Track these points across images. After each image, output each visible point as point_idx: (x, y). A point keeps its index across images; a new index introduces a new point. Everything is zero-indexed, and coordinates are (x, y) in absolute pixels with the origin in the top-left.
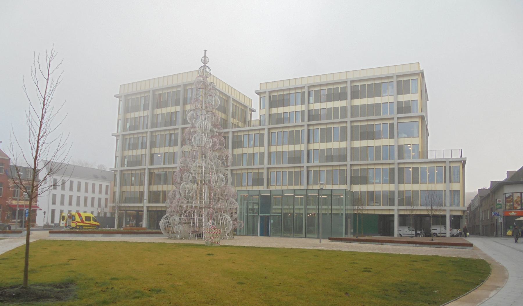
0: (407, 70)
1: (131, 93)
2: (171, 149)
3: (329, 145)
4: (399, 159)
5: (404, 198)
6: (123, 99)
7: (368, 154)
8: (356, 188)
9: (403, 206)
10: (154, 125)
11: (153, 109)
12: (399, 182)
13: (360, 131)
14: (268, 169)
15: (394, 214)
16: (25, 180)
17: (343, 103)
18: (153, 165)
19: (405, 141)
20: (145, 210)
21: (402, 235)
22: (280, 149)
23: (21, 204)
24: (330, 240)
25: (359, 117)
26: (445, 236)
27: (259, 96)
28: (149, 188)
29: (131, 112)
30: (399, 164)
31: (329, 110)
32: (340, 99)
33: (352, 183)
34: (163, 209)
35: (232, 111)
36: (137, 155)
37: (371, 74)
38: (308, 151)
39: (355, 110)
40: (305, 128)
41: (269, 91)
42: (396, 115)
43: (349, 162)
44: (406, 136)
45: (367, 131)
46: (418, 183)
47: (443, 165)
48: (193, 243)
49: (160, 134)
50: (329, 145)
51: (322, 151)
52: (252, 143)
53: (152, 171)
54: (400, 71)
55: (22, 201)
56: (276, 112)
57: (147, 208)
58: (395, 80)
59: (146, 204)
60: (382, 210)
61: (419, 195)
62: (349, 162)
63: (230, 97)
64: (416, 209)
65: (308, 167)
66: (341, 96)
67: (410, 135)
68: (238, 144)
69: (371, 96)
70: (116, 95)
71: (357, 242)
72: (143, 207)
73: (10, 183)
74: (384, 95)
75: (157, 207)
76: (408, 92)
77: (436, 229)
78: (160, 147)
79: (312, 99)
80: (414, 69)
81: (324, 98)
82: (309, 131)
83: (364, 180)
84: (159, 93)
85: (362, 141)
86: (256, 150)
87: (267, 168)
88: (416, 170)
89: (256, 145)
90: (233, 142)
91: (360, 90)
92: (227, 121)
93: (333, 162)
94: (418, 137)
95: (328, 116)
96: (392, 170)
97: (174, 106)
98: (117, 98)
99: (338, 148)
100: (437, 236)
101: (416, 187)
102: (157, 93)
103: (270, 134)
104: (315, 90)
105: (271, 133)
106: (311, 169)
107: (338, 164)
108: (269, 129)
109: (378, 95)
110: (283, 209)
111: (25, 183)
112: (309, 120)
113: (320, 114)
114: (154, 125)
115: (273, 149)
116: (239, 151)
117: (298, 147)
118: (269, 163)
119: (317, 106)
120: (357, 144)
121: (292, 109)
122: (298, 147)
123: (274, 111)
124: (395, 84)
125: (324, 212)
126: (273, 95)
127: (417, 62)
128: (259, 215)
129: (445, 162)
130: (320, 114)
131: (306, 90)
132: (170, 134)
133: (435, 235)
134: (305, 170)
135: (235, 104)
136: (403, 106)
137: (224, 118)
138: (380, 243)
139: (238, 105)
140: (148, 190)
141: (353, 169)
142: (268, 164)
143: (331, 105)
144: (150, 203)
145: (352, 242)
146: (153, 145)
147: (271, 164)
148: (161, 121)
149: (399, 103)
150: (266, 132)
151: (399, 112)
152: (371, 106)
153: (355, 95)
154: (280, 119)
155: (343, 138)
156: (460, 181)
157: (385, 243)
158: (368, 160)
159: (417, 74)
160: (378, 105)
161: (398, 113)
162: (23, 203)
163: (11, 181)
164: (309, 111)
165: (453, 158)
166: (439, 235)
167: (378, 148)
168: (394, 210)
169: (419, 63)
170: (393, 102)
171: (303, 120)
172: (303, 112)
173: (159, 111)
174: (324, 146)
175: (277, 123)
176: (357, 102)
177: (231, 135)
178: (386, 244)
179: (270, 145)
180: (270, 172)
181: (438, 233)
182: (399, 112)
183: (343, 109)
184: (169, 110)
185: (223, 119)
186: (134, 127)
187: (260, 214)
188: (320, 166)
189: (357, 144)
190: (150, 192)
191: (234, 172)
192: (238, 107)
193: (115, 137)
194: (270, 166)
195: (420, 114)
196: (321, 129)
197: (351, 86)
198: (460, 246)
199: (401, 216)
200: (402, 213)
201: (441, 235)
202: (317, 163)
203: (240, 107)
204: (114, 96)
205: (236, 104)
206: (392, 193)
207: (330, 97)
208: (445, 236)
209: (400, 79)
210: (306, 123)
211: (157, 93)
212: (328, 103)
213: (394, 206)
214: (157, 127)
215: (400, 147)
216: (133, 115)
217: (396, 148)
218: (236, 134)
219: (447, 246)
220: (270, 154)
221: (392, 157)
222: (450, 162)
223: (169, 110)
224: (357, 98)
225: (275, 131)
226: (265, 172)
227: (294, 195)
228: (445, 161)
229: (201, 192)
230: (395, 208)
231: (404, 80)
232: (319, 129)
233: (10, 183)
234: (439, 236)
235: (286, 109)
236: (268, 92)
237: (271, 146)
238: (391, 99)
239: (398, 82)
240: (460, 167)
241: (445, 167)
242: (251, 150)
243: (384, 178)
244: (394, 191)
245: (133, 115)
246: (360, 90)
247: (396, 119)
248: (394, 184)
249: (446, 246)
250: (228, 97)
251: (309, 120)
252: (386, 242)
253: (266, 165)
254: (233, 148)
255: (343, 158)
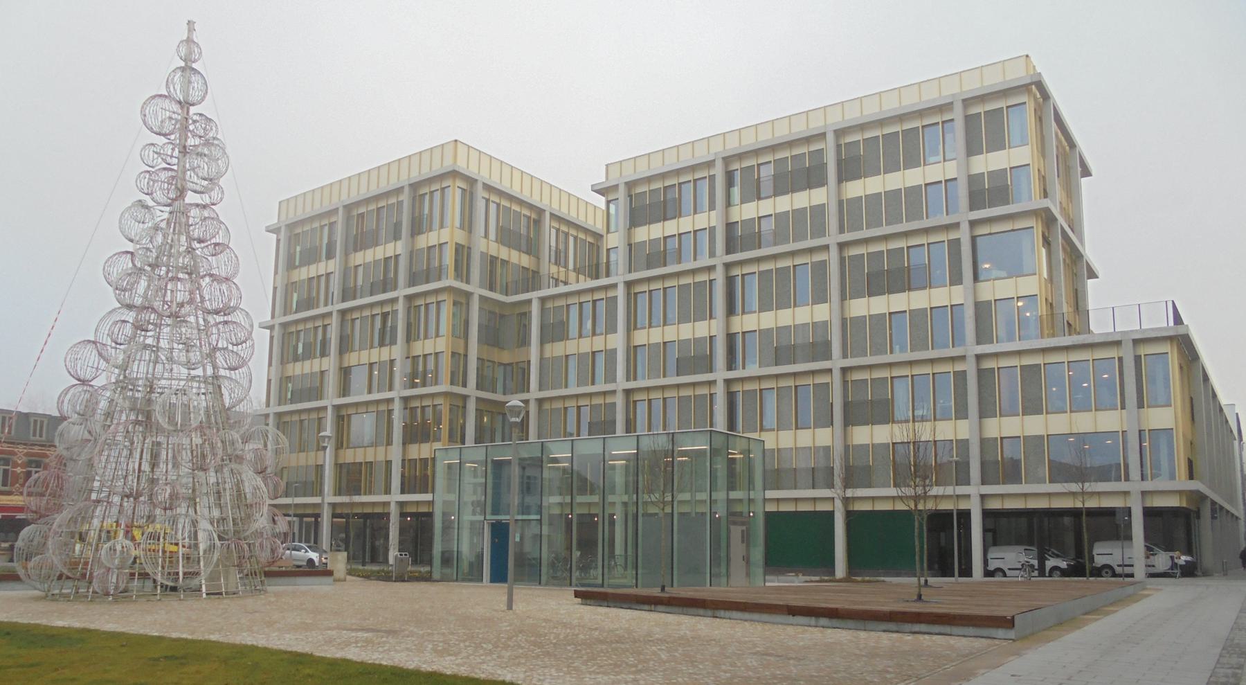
0: (993, 81)
1: (303, 217)
2: (385, 354)
3: (785, 317)
4: (978, 343)
5: (999, 461)
6: (621, 194)
7: (891, 335)
8: (862, 435)
9: (999, 484)
10: (347, 294)
11: (346, 254)
12: (984, 413)
13: (866, 271)
14: (628, 392)
15: (970, 510)
16: (25, 444)
17: (818, 196)
18: (349, 395)
19: (996, 289)
20: (394, 511)
21: (1008, 572)
22: (656, 336)
23: (14, 503)
24: (579, 600)
25: (863, 229)
26: (1132, 576)
27: (604, 198)
28: (336, 456)
29: (301, 265)
30: (979, 358)
31: (781, 218)
32: (810, 186)
33: (848, 422)
34: (378, 510)
35: (557, 248)
36: (312, 373)
37: (891, 106)
38: (731, 338)
39: (849, 212)
40: (719, 276)
41: (626, 183)
42: (965, 215)
43: (837, 362)
44: (1004, 274)
45: (886, 268)
46: (1039, 412)
47: (1113, 353)
48: (20, 620)
49: (361, 317)
50: (785, 317)
51: (765, 334)
52: (589, 324)
53: (344, 412)
54: (973, 86)
55: (16, 497)
56: (646, 238)
57: (331, 508)
58: (958, 114)
59: (329, 497)
60: (1025, 495)
61: (1044, 450)
62: (837, 362)
63: (545, 211)
64: (1090, 490)
65: (728, 382)
66: (811, 177)
67: (1016, 271)
68: (554, 331)
69: (892, 167)
70: (269, 226)
71: (646, 607)
72: (387, 504)
73: (17, 454)
74: (932, 159)
75: (417, 503)
76: (998, 143)
77: (1104, 553)
78: (360, 350)
79: (736, 192)
80: (1017, 75)
81: (767, 187)
82: (730, 281)
83: (881, 412)
84: (359, 212)
85: (874, 300)
86: (598, 343)
87: (624, 390)
88: (1031, 373)
89: (598, 331)
90: (543, 327)
91: (862, 153)
92: (538, 272)
93: (794, 363)
94: (1035, 274)
95: (779, 237)
96: (961, 377)
97: (391, 242)
98: (271, 234)
99: (809, 323)
100: (1114, 575)
101: (1035, 425)
102: (356, 214)
103: (631, 298)
104: (743, 166)
105: (636, 294)
106: (737, 388)
107: (807, 369)
108: (629, 284)
109: (913, 161)
110: (574, 504)
111: (25, 451)
112: (729, 251)
113: (906, 265)
114: (347, 294)
115: (640, 338)
116: (557, 349)
117: (702, 329)
118: (631, 374)
119: (746, 211)
120: (860, 307)
121: (686, 224)
122: (702, 329)
123: (643, 234)
124: (959, 125)
125: (686, 509)
126: (637, 192)
127: (454, 139)
128: (485, 519)
129: (1117, 343)
130: (906, 265)
131: (718, 171)
132: (382, 313)
133: (1107, 573)
134: (720, 391)
135: (564, 228)
136: (987, 187)
137: (526, 265)
138: (710, 612)
139: (573, 232)
140: (333, 463)
141: (850, 380)
142: (628, 379)
143: (784, 204)
144: (340, 495)
145: (634, 607)
146: (345, 345)
147: (635, 379)
148: (363, 282)
149: (974, 180)
150: (620, 292)
151: (974, 205)
152: (893, 195)
153: (850, 168)
154: (657, 254)
155: (820, 296)
156: (1169, 398)
157: (722, 613)
158: (891, 352)
159: (1024, 88)
160: (913, 192)
161: (972, 209)
162: (21, 501)
163: (21, 450)
164: (730, 226)
165: (1146, 330)
166: (1118, 570)
167: (917, 316)
168: (968, 496)
169: (1027, 56)
170: (955, 179)
171: (712, 254)
172: (712, 230)
173: (359, 258)
174: (768, 320)
175: (649, 266)
176: (855, 189)
177: (535, 309)
178: (728, 614)
179: (632, 326)
180: (635, 402)
181: (1118, 566)
182: (974, 205)
183: (819, 211)
184: (379, 252)
185: (523, 267)
186: (308, 303)
187: (488, 517)
188: (760, 378)
189: (860, 307)
190: (339, 467)
191: (547, 406)
192: (576, 238)
193: (268, 331)
194: (632, 385)
195: (1038, 203)
196: (761, 273)
197: (838, 146)
198: (998, 627)
199: (989, 515)
200: (995, 505)
201: (1126, 572)
202: (753, 370)
203: (581, 236)
204: (264, 228)
205: (575, 234)
206: (963, 445)
207: (787, 182)
208: (1132, 576)
209: (974, 110)
210: (721, 258)
211: (355, 213)
212: (778, 199)
213: (969, 484)
214: (355, 298)
215: (983, 311)
216: (303, 274)
217: (969, 313)
218: (549, 305)
219: (923, 627)
220: (632, 351)
221: (957, 339)
222: (1136, 342)
223: (379, 252)
224: (856, 176)
225: (644, 288)
226: (619, 400)
227: (572, 456)
228: (1120, 339)
229: (155, 447)
230: (974, 489)
231: (985, 112)
232: (755, 273)
233: (17, 454)
234: (1120, 576)
235: (671, 227)
236: (623, 185)
237: (635, 328)
238: (952, 170)
239: (970, 120)
240: (1170, 355)
241: (1120, 359)
242: (585, 346)
243: (942, 401)
244: (968, 440)
245: (303, 274)
246: (862, 153)
247: (965, 227)
248: (967, 418)
249: (917, 627)
250: (540, 211)
251: (729, 251)
252: (725, 609)
253: (621, 383)
254: (542, 342)
255: (821, 349)
